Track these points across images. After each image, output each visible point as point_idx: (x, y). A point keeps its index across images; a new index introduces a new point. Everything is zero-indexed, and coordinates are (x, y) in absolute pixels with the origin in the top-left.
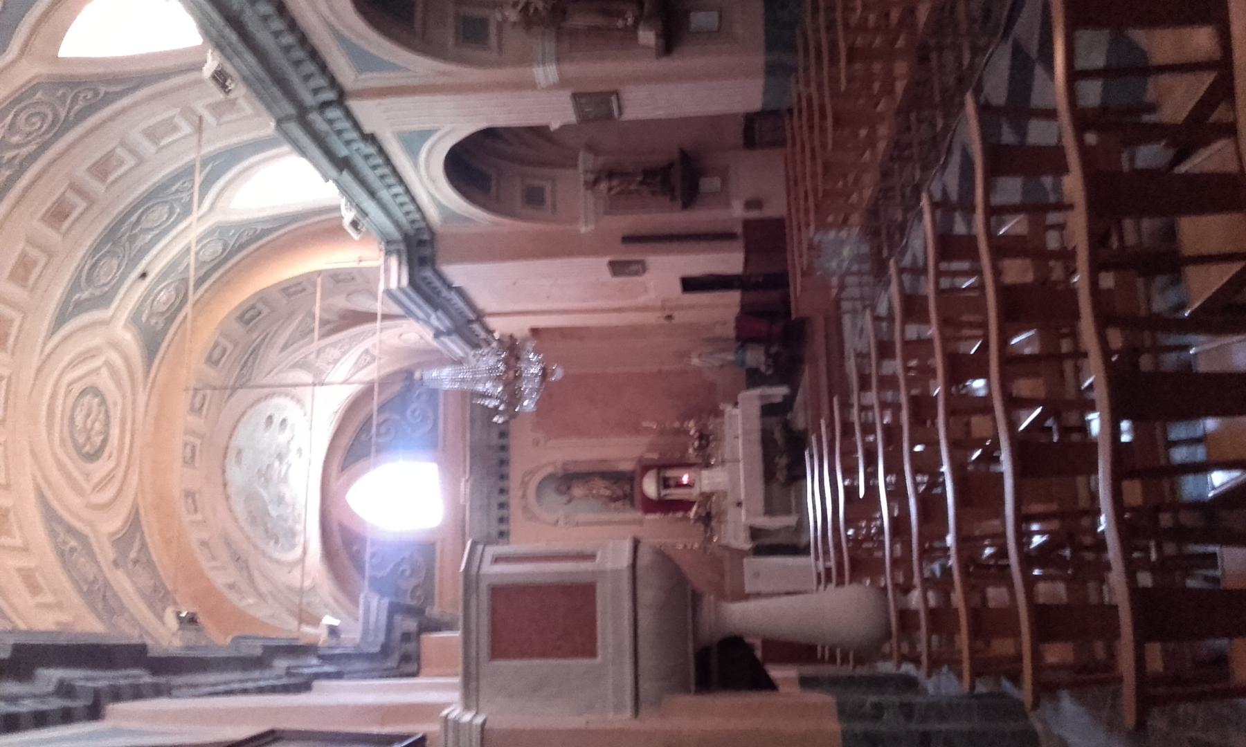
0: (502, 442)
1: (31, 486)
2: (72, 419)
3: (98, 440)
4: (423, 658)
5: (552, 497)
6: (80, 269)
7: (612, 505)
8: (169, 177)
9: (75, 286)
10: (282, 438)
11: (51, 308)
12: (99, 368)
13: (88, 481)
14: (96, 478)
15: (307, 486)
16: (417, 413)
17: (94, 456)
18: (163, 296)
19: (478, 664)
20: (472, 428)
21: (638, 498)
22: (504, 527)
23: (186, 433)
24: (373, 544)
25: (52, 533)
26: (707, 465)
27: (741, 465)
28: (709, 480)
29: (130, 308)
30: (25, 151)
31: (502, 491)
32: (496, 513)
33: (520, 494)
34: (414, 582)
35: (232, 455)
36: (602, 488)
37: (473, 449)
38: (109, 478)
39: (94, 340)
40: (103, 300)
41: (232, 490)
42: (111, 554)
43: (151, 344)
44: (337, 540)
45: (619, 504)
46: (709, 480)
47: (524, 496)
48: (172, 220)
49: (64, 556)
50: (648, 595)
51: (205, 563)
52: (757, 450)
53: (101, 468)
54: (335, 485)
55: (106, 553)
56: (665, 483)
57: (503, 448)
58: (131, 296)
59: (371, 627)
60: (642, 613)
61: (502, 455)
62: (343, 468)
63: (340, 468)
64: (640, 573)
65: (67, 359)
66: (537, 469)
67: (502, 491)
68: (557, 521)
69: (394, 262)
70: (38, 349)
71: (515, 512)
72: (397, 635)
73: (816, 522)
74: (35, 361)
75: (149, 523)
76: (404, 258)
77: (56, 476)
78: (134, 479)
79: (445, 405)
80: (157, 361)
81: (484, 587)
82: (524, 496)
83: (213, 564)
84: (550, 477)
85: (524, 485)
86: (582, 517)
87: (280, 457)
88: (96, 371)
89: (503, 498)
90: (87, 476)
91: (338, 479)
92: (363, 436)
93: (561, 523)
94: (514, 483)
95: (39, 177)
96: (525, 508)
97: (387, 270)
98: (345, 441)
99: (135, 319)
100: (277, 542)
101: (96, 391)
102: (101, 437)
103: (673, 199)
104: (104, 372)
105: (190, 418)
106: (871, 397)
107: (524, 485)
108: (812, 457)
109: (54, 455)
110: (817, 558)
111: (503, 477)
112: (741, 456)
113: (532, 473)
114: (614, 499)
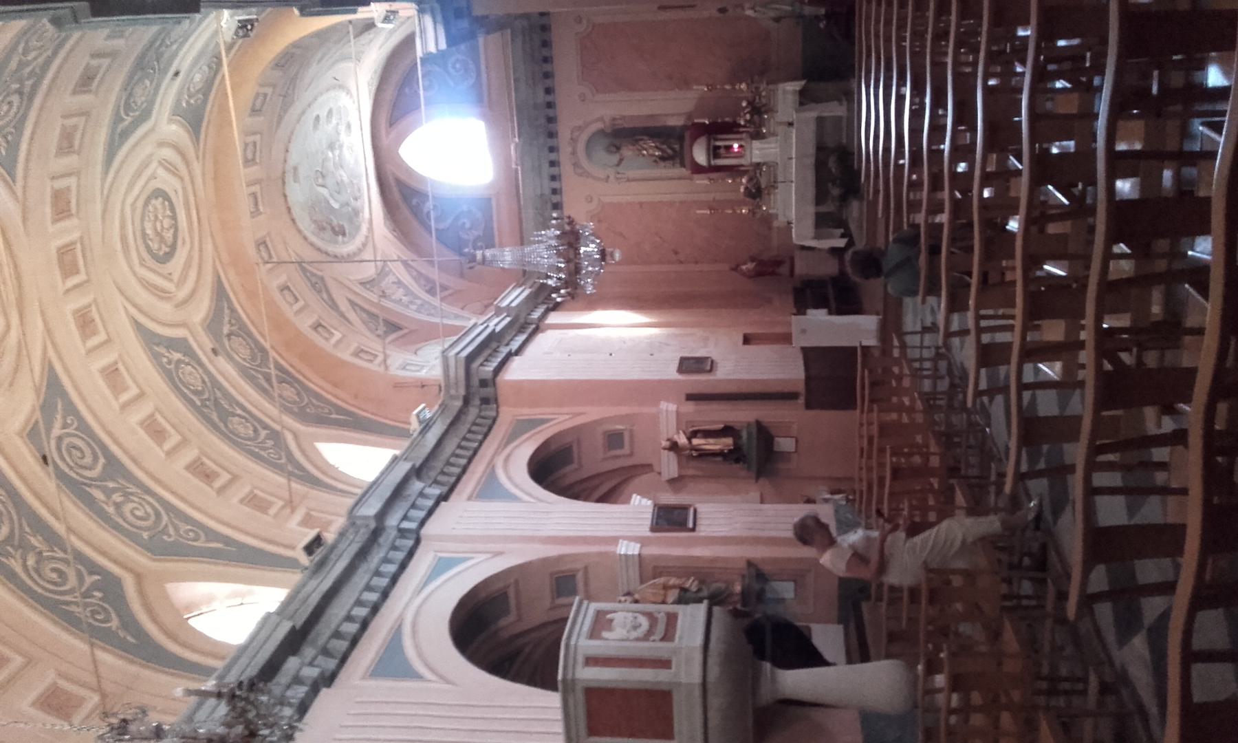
0: (549, 98)
1: (125, 320)
2: (144, 235)
3: (169, 235)
4: (501, 399)
5: (601, 154)
6: (119, 99)
7: (662, 164)
8: (262, 463)
9: (117, 119)
10: (329, 128)
11: (100, 153)
12: (155, 172)
13: (171, 280)
14: (176, 277)
15: (361, 129)
16: (458, 66)
17: (169, 255)
18: (198, 78)
19: (574, 668)
20: (516, 90)
21: (687, 161)
22: (556, 185)
23: (248, 186)
24: (434, 197)
25: (156, 357)
26: (758, 136)
27: (793, 185)
28: (758, 152)
29: (168, 107)
30: (41, 60)
31: (552, 149)
32: (547, 170)
33: (570, 149)
34: (475, 233)
35: (289, 178)
36: (651, 148)
37: (519, 111)
38: (187, 265)
39: (147, 149)
40: (146, 114)
41: (296, 212)
42: (208, 344)
43: (193, 119)
44: (396, 195)
45: (668, 163)
46: (758, 152)
47: (574, 153)
48: (242, 334)
49: (172, 377)
50: (715, 702)
51: (289, 311)
52: (810, 176)
53: (176, 264)
54: (385, 142)
55: (202, 343)
56: (714, 152)
57: (550, 105)
58: (169, 94)
59: (452, 380)
60: (711, 714)
61: (550, 112)
62: (391, 124)
63: (388, 124)
64: (710, 686)
65: (123, 190)
66: (587, 125)
67: (552, 149)
68: (608, 177)
69: (428, 21)
70: (98, 193)
71: (566, 169)
72: (475, 382)
73: (860, 27)
74: (98, 208)
75: (231, 281)
76: (439, 18)
77: (144, 297)
78: (209, 247)
79: (486, 60)
80: (202, 137)
81: (579, 688)
82: (574, 153)
83: (296, 307)
84: (601, 133)
85: (574, 140)
86: (631, 174)
87: (331, 147)
88: (153, 177)
89: (553, 156)
90: (168, 277)
91: (388, 133)
92: (407, 90)
93: (612, 177)
94: (564, 132)
95: (60, 68)
96: (576, 165)
97: (423, 31)
98: (389, 94)
99: (177, 112)
100: (344, 234)
101: (159, 193)
102: (172, 231)
103: (749, 469)
104: (161, 172)
105: (249, 170)
106: (927, 385)
107: (574, 140)
108: (868, 87)
109: (122, 210)
110: (862, 412)
111: (552, 135)
112: (794, 156)
113: (580, 129)
114: (663, 158)
